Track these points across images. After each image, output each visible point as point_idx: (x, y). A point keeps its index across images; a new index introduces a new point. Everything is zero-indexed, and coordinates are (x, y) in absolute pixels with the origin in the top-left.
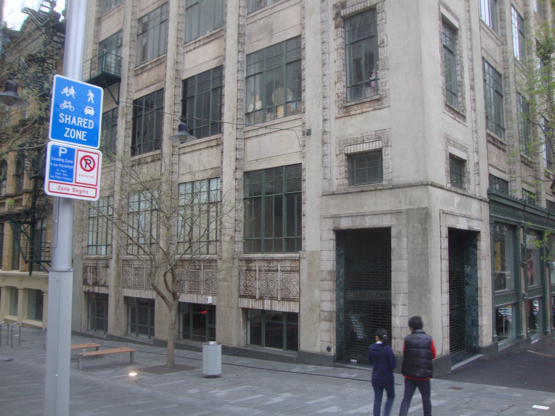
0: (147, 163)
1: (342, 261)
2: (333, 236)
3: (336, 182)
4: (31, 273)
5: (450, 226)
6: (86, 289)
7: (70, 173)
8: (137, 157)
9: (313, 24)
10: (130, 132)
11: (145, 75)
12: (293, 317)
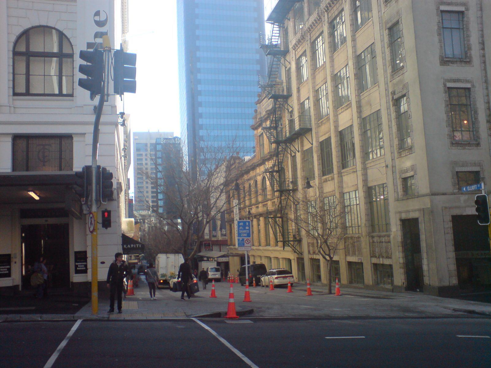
0: (329, 180)
2: (399, 223)
4: (284, 248)
5: (452, 215)
6: (310, 256)
7: (244, 244)
8: (325, 177)
9: (384, 101)
12: (391, 266)
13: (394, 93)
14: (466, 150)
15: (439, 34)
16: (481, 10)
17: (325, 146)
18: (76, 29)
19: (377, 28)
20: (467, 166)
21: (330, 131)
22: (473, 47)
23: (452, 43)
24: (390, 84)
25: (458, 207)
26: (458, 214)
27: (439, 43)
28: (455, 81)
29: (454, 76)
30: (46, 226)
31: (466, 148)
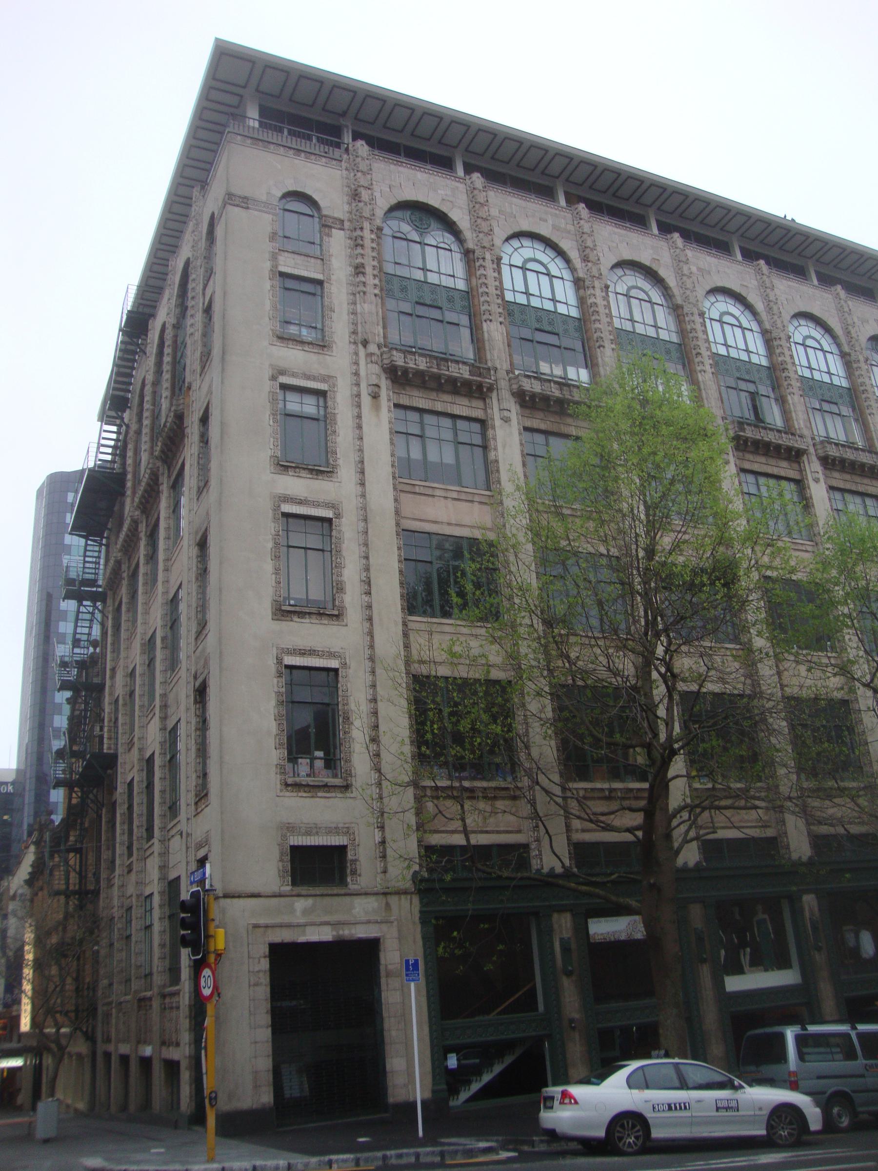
14: (317, 799)
15: (277, 557)
16: (365, 520)
20: (317, 833)
22: (348, 588)
23: (306, 576)
25: (289, 926)
26: (286, 941)
27: (274, 576)
28: (303, 653)
30: (286, 1004)
31: (320, 794)
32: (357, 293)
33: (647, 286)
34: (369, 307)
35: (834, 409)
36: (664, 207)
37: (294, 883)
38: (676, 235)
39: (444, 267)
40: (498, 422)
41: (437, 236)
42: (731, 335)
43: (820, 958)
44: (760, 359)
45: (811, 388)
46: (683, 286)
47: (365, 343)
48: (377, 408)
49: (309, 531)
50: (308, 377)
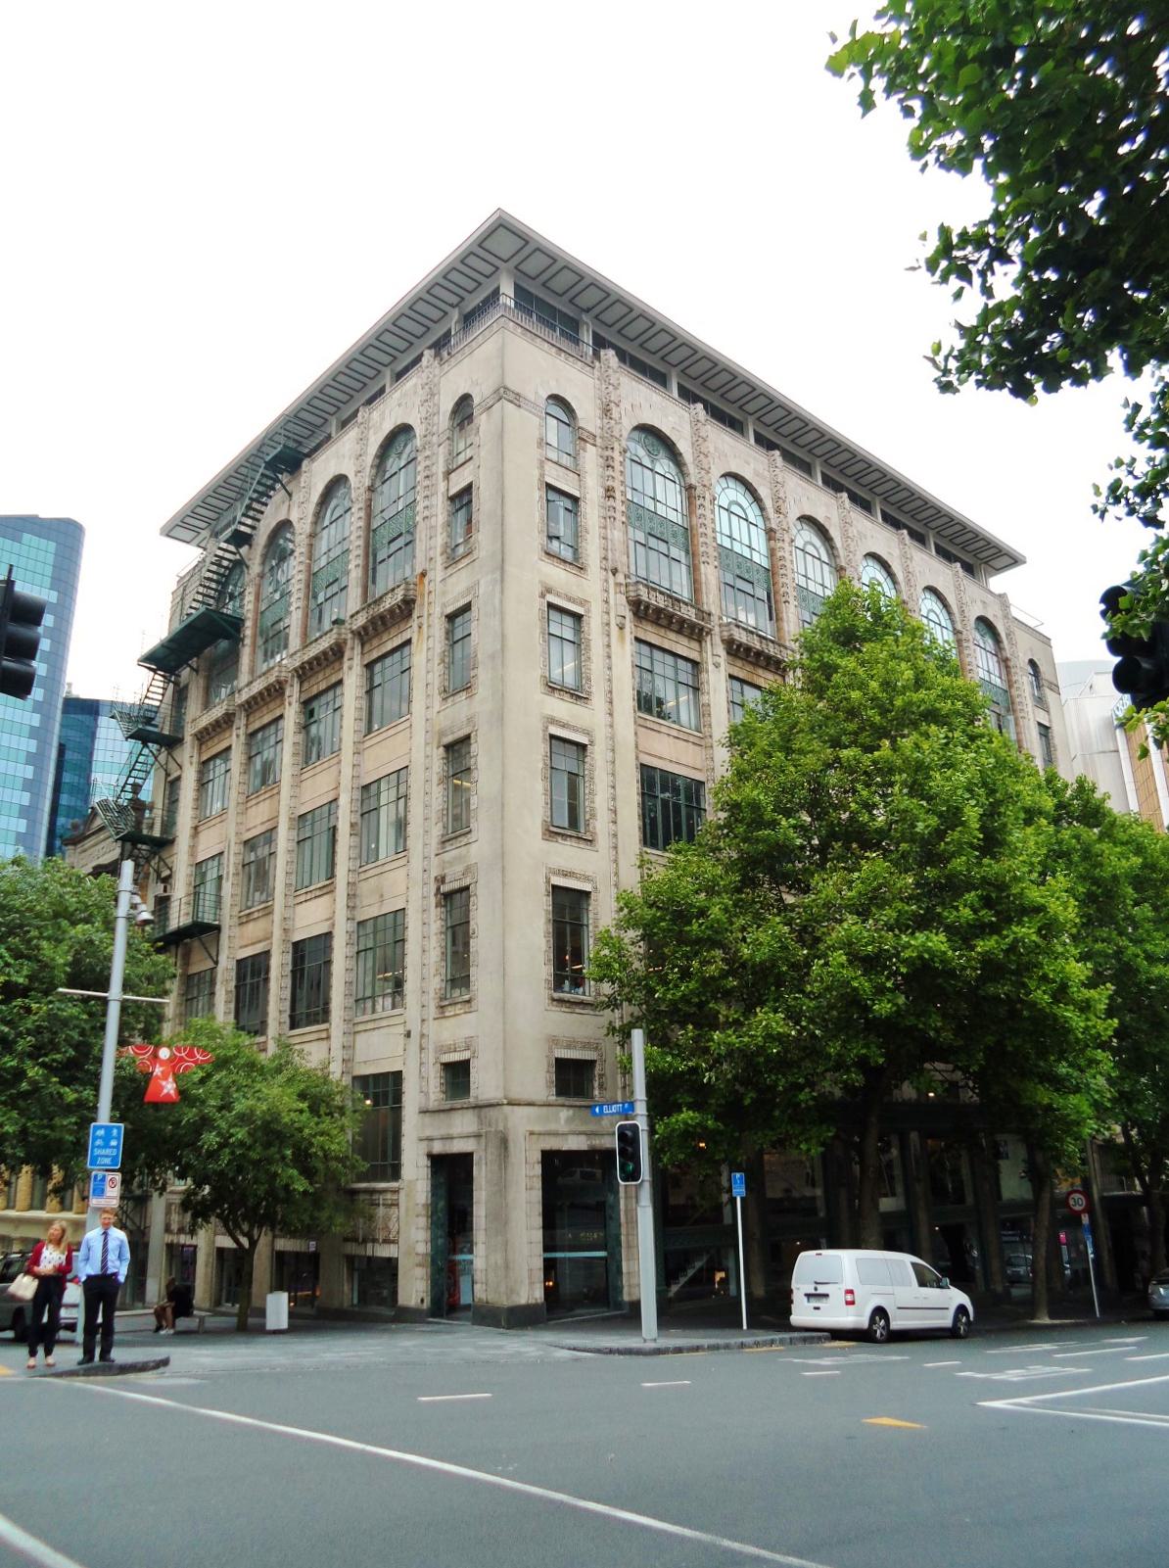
1: (442, 1192)
2: (425, 1162)
3: (432, 1097)
6: (168, 1238)
9: (416, 894)
10: (232, 1006)
11: (251, 925)
13: (442, 880)
17: (252, 971)
18: (424, 1112)
19: (419, 737)
21: (268, 937)
24: (435, 861)
25: (556, 1134)
28: (566, 874)
29: (567, 866)
32: (608, 518)
33: (818, 543)
34: (617, 535)
35: (663, 547)
36: (552, 284)
37: (559, 1093)
38: (777, 453)
39: (669, 500)
40: (711, 667)
41: (664, 466)
42: (735, 529)
43: (919, 1188)
44: (761, 559)
45: (639, 518)
46: (847, 548)
47: (615, 572)
48: (622, 638)
49: (568, 753)
50: (570, 599)
